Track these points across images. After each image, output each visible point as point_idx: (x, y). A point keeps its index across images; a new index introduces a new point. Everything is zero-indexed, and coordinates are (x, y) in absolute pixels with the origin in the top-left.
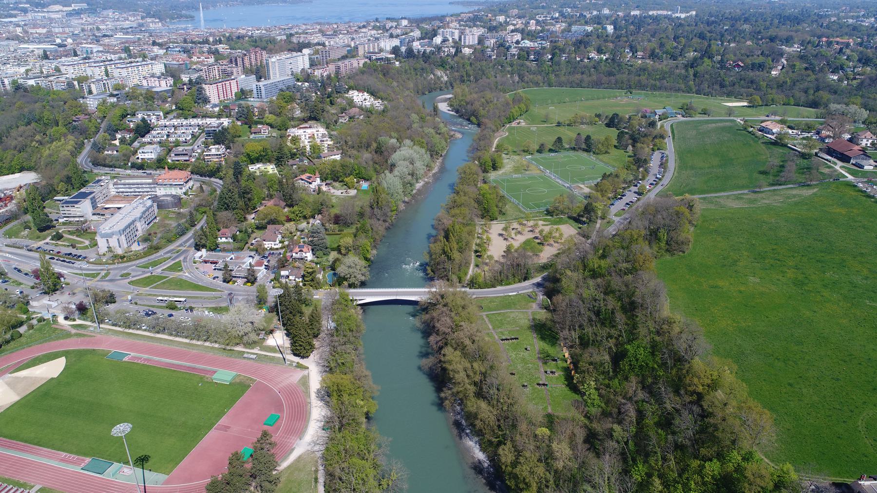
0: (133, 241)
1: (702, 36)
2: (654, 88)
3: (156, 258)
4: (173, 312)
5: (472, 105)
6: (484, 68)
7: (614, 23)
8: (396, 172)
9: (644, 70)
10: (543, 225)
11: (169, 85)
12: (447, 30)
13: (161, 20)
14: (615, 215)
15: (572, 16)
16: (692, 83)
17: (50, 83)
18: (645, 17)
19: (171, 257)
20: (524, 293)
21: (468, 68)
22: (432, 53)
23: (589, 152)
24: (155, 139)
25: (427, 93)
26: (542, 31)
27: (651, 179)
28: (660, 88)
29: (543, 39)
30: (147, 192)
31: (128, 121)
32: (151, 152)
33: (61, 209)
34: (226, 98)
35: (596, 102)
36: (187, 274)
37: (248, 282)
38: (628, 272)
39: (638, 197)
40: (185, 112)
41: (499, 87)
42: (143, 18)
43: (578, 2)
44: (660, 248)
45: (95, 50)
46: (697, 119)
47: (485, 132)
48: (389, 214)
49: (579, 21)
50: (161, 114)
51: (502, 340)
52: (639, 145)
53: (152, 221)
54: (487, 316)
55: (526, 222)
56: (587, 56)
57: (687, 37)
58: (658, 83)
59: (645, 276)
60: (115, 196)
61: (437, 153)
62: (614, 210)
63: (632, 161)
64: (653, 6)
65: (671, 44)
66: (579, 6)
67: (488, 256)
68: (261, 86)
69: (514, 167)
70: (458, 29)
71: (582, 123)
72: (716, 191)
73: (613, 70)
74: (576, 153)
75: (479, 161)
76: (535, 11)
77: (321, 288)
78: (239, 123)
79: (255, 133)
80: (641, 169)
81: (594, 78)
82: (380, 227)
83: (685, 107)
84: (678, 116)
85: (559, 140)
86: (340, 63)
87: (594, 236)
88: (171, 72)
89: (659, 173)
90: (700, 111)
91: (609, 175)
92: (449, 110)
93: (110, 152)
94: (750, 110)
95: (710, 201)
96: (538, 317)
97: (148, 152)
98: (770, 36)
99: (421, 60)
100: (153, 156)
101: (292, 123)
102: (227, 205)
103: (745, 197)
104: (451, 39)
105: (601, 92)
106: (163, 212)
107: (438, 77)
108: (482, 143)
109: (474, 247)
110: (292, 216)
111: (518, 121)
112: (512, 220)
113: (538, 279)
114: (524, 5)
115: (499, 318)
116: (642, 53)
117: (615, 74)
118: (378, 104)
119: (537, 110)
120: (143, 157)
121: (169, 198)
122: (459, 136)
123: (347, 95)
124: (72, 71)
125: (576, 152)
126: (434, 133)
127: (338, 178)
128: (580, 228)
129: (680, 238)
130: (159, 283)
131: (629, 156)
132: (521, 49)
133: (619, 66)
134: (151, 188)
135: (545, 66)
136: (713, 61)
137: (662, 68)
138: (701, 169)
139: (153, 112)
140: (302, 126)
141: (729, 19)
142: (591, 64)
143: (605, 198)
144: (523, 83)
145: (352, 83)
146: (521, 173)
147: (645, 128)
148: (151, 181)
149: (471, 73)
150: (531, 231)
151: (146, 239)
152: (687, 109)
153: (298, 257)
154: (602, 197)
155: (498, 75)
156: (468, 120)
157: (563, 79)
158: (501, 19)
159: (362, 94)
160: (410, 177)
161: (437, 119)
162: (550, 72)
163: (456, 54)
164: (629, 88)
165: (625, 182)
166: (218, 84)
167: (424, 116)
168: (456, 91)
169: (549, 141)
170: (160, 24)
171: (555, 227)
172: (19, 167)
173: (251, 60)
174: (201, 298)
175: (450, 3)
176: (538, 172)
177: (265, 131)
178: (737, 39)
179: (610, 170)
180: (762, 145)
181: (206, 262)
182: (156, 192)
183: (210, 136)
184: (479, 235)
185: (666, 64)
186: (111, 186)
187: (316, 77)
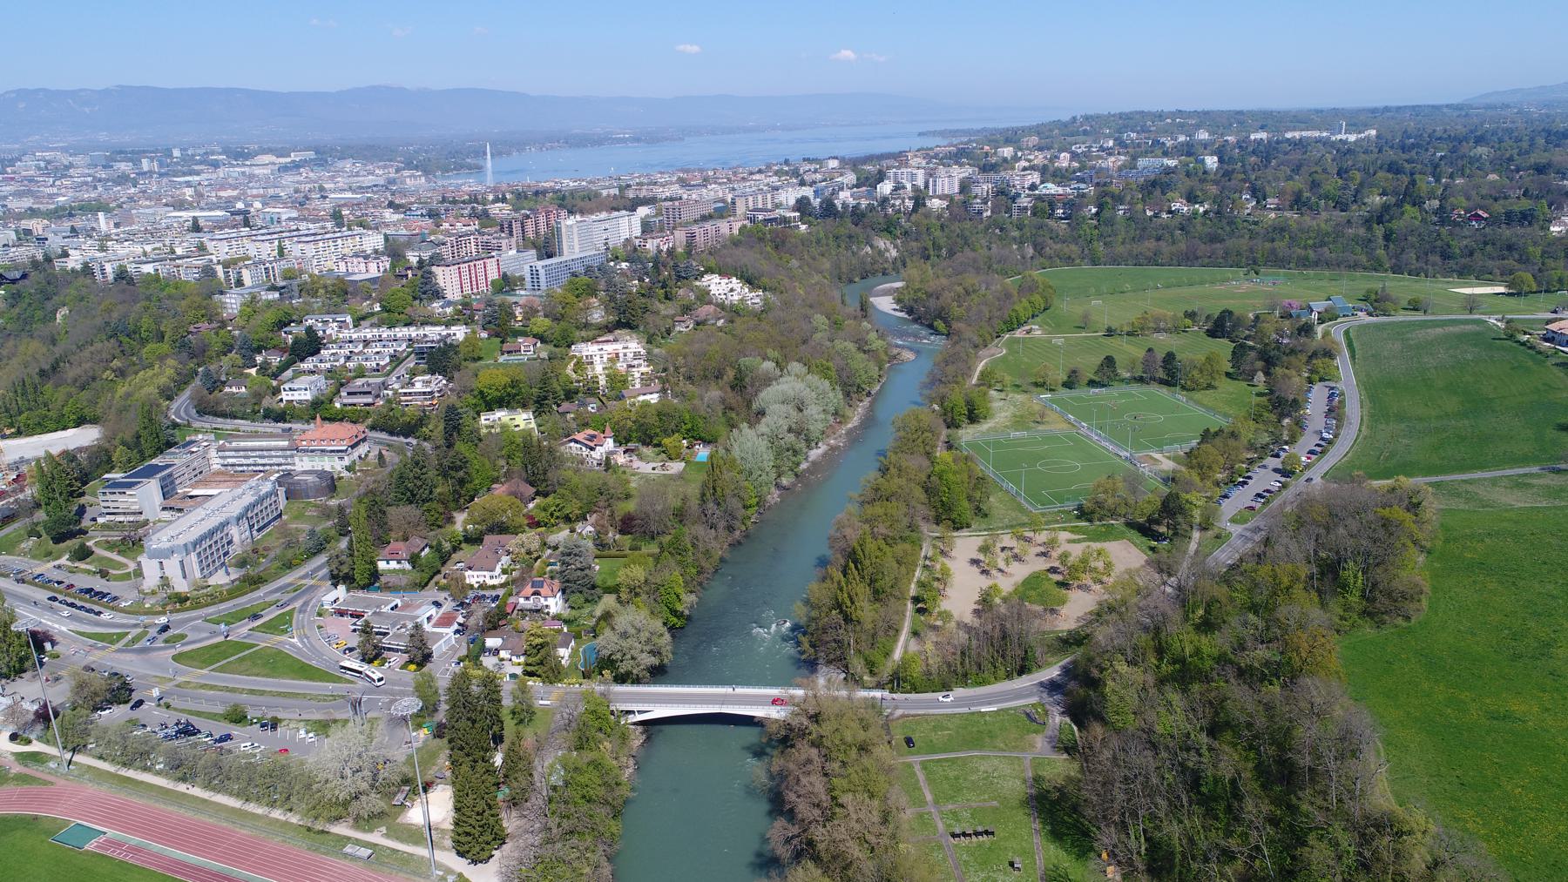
0: (217, 564)
1: (1394, 168)
2: (1304, 263)
3: (247, 603)
4: (235, 731)
5: (938, 298)
6: (967, 233)
7: (1220, 153)
8: (763, 427)
9: (1282, 230)
10: (1069, 541)
11: (382, 269)
12: (904, 170)
13: (426, 172)
14: (1233, 521)
15: (1139, 145)
16: (1381, 252)
17: (175, 269)
18: (1278, 142)
19: (278, 601)
20: (1015, 709)
21: (938, 233)
22: (871, 208)
23: (1175, 385)
24: (323, 365)
25: (857, 279)
26: (1080, 170)
27: (1308, 441)
28: (1316, 264)
29: (1081, 180)
30: (279, 465)
31: (285, 333)
32: (306, 390)
33: (101, 498)
34: (475, 291)
35: (1186, 291)
36: (295, 640)
37: (411, 662)
38: (1270, 672)
39: (1283, 479)
40: (392, 315)
41: (995, 266)
42: (398, 171)
43: (1149, 123)
44: (1347, 608)
45: (284, 217)
46: (1401, 318)
47: (958, 347)
48: (741, 513)
49: (1152, 152)
50: (349, 319)
51: (954, 835)
52: (1278, 371)
53: (269, 523)
54: (924, 765)
55: (1031, 534)
56: (1166, 208)
57: (1365, 170)
58: (1311, 254)
59: (1314, 688)
60: (218, 473)
61: (859, 389)
62: (1229, 508)
63: (1266, 403)
64: (1292, 125)
65: (1332, 184)
66: (1152, 129)
67: (940, 614)
68: (539, 268)
69: (1015, 416)
70: (924, 168)
71: (1158, 330)
72: (1462, 468)
73: (1220, 231)
74: (1144, 388)
75: (941, 405)
76: (1069, 139)
77: (560, 681)
78: (484, 335)
79: (509, 352)
80: (1286, 421)
81: (1183, 246)
82: (717, 545)
83: (1373, 297)
84: (1359, 313)
85: (1109, 361)
86: (695, 228)
87: (1184, 568)
88: (394, 250)
89: (1327, 428)
90: (1404, 303)
91: (1216, 434)
92: (894, 310)
93: (234, 390)
94: (1512, 301)
95: (1453, 492)
96: (1046, 773)
97: (300, 389)
98: (1535, 164)
99: (848, 220)
100: (307, 396)
101: (583, 333)
102: (412, 492)
103: (1534, 481)
104: (909, 186)
105: (1196, 272)
106: (297, 505)
107: (880, 251)
108: (951, 369)
109: (913, 590)
110: (541, 516)
111: (1027, 328)
112: (1002, 528)
113: (1052, 672)
114: (1051, 130)
115: (952, 774)
116: (1276, 201)
117: (1224, 240)
118: (754, 298)
119: (1067, 307)
120: (290, 398)
121: (310, 478)
122: (908, 355)
123: (698, 283)
124: (227, 250)
125: (1145, 386)
126: (854, 350)
127: (651, 438)
128: (1153, 549)
129: (1395, 584)
130: (232, 659)
131: (1259, 395)
132: (1040, 198)
133: (1231, 223)
134: (286, 457)
135: (1085, 227)
136: (1421, 210)
137: (1318, 225)
138: (1420, 419)
139: (334, 316)
140: (600, 339)
141: (1445, 139)
142: (1176, 222)
143: (1209, 483)
144: (1042, 260)
145: (712, 262)
146: (1028, 429)
147: (1290, 338)
148: (286, 443)
149: (942, 241)
150: (1044, 554)
151: (242, 563)
152: (1376, 301)
153: (529, 607)
154: (1202, 479)
155: (994, 246)
156: (931, 326)
157: (1120, 249)
158: (1007, 152)
159: (726, 281)
160: (791, 438)
161: (865, 323)
162: (1095, 238)
163: (915, 209)
164: (1254, 263)
165: (1251, 447)
166: (461, 266)
167: (840, 317)
168: (909, 275)
169: (1089, 364)
170: (423, 179)
171: (1096, 546)
172: (74, 417)
173: (537, 226)
174: (304, 695)
175: (920, 134)
176: (1065, 426)
177: (528, 349)
178: (1468, 171)
179: (1217, 422)
180: (1556, 370)
181: (341, 613)
182: (294, 464)
183: (424, 358)
184: (927, 562)
185: (1326, 218)
186: (213, 453)
187: (648, 251)
